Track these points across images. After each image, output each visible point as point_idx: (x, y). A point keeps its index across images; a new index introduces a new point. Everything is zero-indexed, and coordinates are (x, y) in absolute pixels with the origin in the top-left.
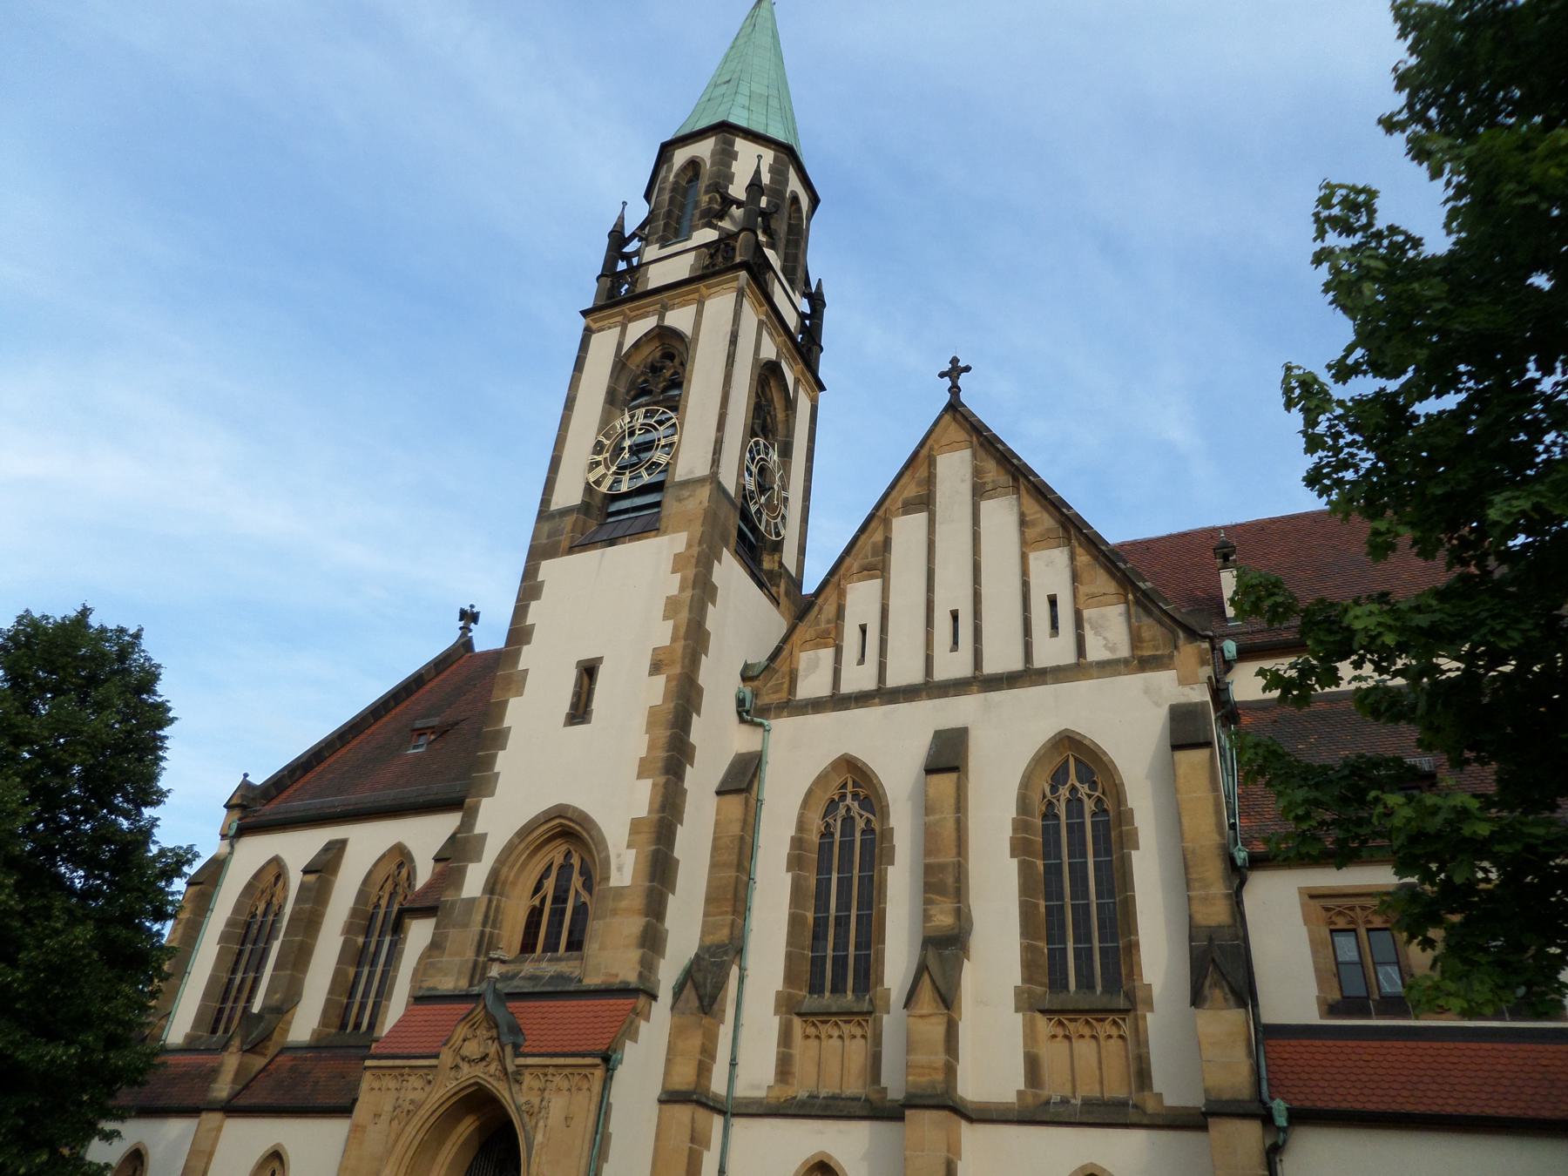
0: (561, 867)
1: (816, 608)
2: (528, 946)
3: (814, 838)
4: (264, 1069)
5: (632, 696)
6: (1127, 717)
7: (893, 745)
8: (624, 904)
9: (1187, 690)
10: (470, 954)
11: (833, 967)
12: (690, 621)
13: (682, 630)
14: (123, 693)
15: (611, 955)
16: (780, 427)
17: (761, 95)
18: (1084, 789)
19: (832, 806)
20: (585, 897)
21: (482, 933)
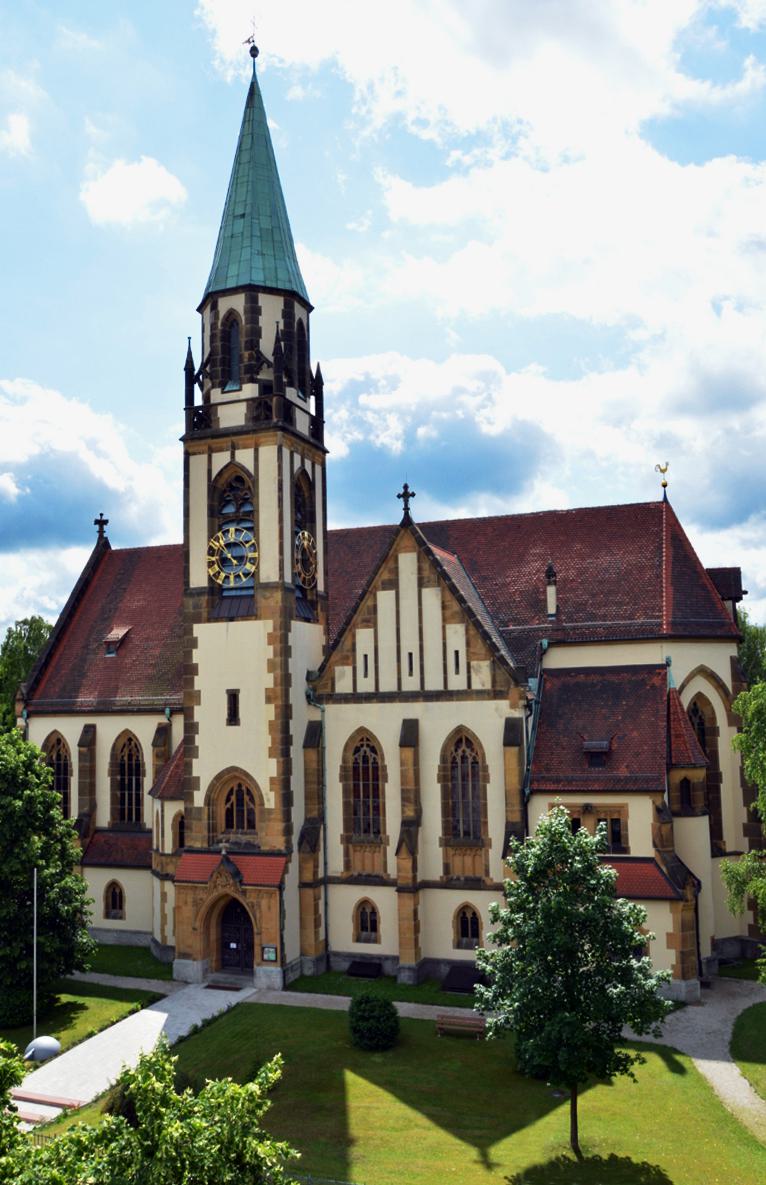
0: (237, 791)
1: (341, 644)
2: (229, 824)
3: (351, 765)
4: (91, 842)
5: (258, 714)
6: (488, 720)
7: (384, 723)
8: (272, 816)
9: (513, 711)
10: (205, 833)
11: (364, 821)
12: (281, 675)
13: (279, 681)
14: (382, 1139)
15: (271, 836)
16: (307, 501)
17: (267, 230)
18: (468, 751)
19: (357, 750)
20: (252, 806)
21: (209, 824)
